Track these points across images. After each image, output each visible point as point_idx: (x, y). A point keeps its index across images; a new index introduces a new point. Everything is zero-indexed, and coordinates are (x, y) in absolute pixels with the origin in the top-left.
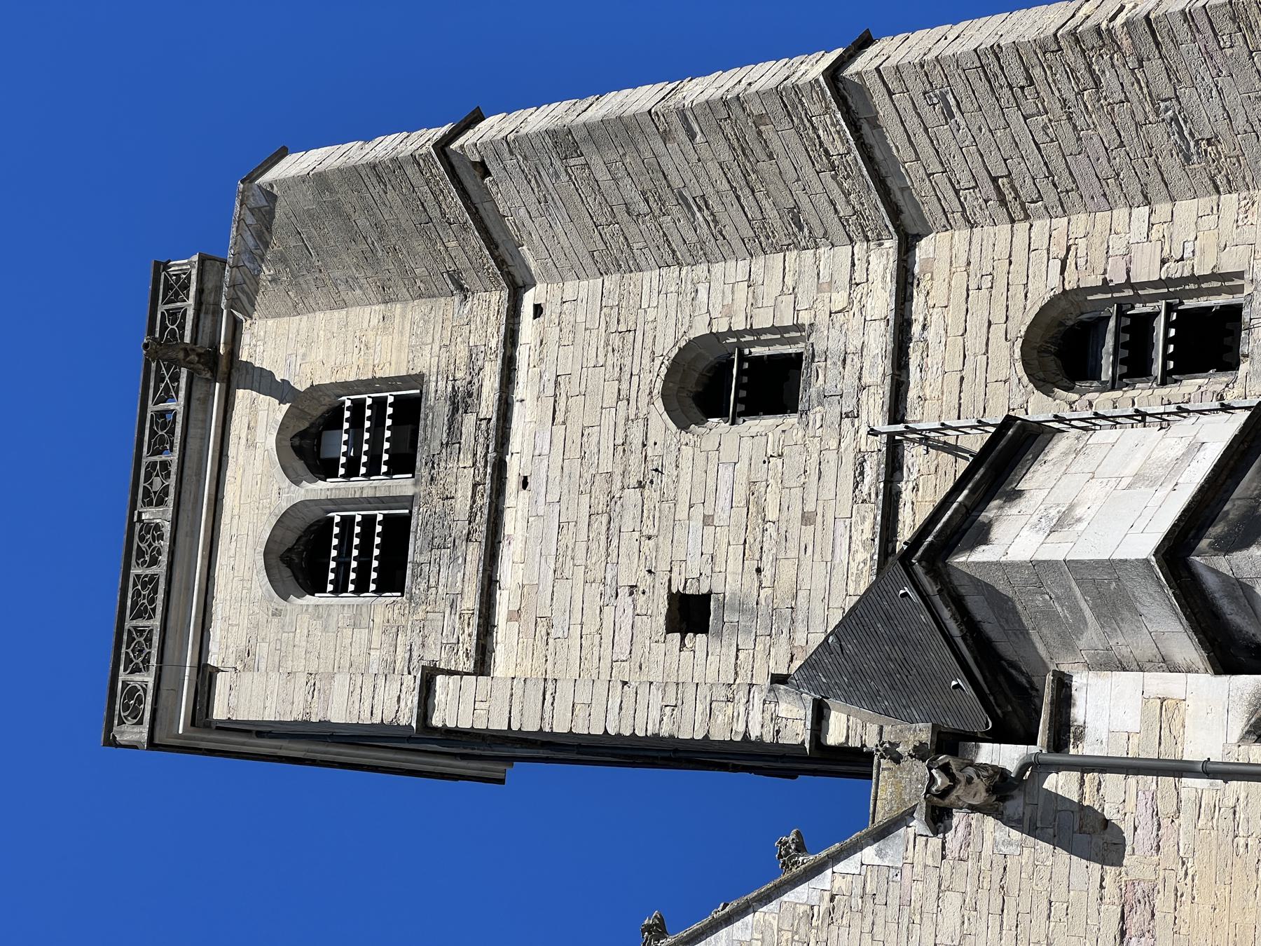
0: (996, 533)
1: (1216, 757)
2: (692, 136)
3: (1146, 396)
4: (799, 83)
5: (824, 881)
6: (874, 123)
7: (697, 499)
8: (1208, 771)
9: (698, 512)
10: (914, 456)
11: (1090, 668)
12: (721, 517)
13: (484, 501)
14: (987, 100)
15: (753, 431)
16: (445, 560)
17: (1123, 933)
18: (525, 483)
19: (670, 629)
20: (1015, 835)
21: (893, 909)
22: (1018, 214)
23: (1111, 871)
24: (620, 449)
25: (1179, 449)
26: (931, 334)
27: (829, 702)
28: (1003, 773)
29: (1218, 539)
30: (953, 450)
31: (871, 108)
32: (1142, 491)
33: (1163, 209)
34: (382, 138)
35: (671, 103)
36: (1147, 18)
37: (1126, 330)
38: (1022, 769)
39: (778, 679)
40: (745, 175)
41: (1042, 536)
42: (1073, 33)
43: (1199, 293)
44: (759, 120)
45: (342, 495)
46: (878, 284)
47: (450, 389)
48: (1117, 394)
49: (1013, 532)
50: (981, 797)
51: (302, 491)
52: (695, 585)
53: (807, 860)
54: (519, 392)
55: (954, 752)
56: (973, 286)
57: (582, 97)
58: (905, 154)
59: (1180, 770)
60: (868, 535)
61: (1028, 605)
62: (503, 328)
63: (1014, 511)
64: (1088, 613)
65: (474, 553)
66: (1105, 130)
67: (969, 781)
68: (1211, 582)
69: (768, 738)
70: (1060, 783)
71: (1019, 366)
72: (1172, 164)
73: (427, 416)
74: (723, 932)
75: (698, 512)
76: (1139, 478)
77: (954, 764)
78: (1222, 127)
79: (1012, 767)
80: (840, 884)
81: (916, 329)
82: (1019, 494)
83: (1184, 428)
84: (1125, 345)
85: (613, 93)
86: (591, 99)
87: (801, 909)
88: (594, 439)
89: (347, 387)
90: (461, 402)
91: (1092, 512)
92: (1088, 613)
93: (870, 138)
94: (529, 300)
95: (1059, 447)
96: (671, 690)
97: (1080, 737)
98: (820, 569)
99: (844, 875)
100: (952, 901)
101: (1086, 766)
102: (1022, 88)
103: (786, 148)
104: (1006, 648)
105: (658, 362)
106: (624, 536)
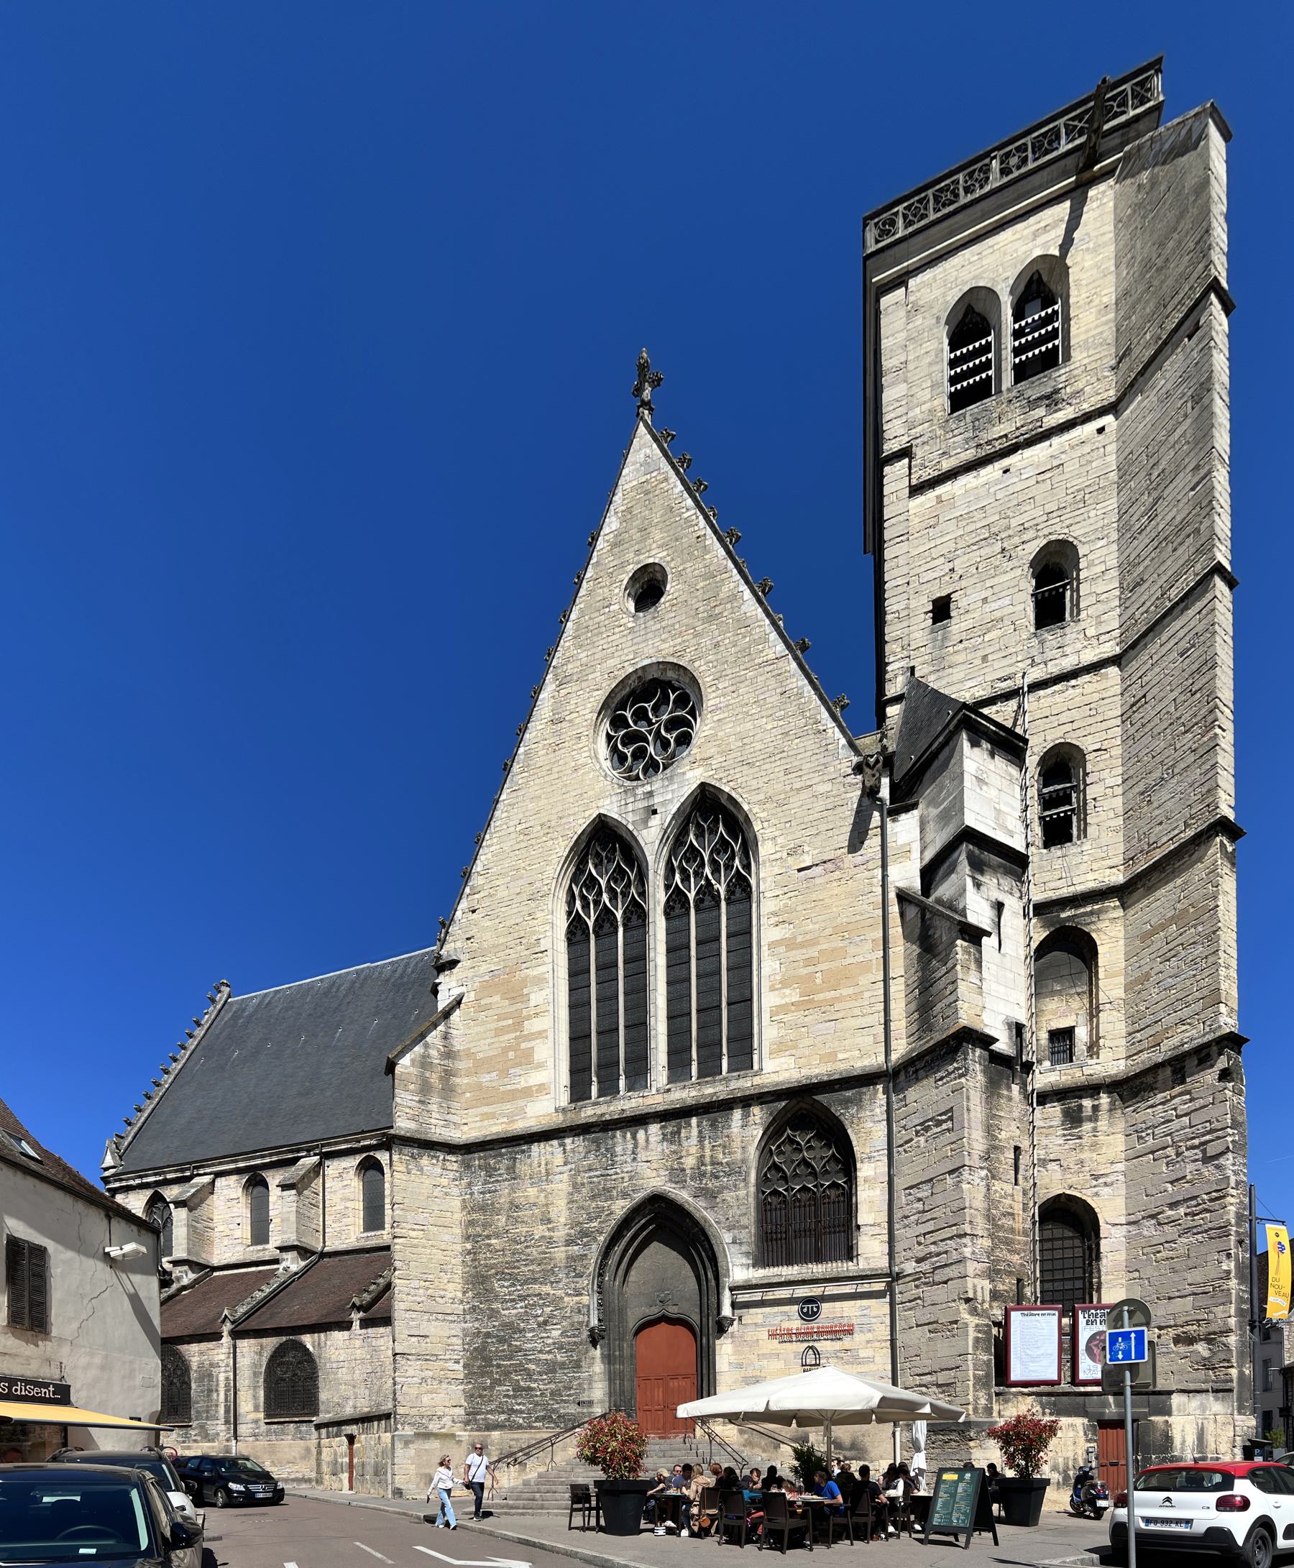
0: (976, 750)
1: (890, 879)
2: (1193, 489)
3: (1035, 811)
4: (1215, 549)
5: (831, 724)
6: (1187, 608)
7: (996, 589)
8: (884, 877)
9: (988, 593)
10: (1013, 704)
11: (921, 817)
12: (987, 608)
13: (998, 446)
14: (1189, 671)
15: (1028, 609)
16: (967, 435)
17: (825, 862)
18: (1006, 471)
19: (934, 602)
20: (855, 806)
21: (823, 761)
22: (1125, 717)
23: (846, 850)
24: (1022, 528)
25: (1010, 827)
26: (1071, 691)
27: (904, 702)
28: (878, 792)
29: (973, 852)
30: (1015, 724)
31: (1193, 604)
32: (993, 814)
33: (1119, 790)
34: (1226, 229)
35: (1216, 462)
36: (1217, 745)
37: (1065, 792)
38: (880, 800)
39: (912, 669)
40: (1165, 539)
41: (974, 773)
42: (1216, 707)
43: (1079, 821)
44: (1197, 531)
45: (1003, 333)
46: (1097, 651)
47: (1060, 386)
48: (1036, 798)
49: (976, 759)
50: (868, 784)
51: (1006, 298)
52: (960, 603)
53: (838, 711)
54: (1056, 441)
55: (884, 766)
56: (1092, 706)
57: (1230, 394)
58: (1164, 637)
59: (884, 866)
60: (977, 695)
61: (945, 779)
62: (1093, 408)
63: (985, 757)
64: (942, 807)
65: (970, 455)
66: (1162, 745)
67: (874, 776)
68: (956, 855)
69: (887, 676)
70: (876, 818)
71: (1052, 744)
72: (1137, 790)
73: (1044, 377)
74: (806, 681)
75: (988, 593)
76: (998, 811)
77: (880, 765)
78: (1155, 805)
79: (880, 795)
80: (830, 731)
81: (1073, 682)
82: (993, 757)
83: (1020, 827)
84: (1058, 795)
85: (1228, 416)
86: (1227, 399)
87: (818, 717)
88: (1028, 508)
89: (1066, 306)
90: (1052, 400)
91: (984, 794)
92: (942, 807)
93: (1176, 611)
94: (1108, 420)
95: (1014, 771)
96: (905, 613)
97: (894, 821)
98: (962, 675)
99: (833, 733)
100: (828, 787)
101: (883, 827)
102: (1176, 750)
103: (1178, 558)
104: (928, 775)
105: (1066, 531)
106: (978, 553)
